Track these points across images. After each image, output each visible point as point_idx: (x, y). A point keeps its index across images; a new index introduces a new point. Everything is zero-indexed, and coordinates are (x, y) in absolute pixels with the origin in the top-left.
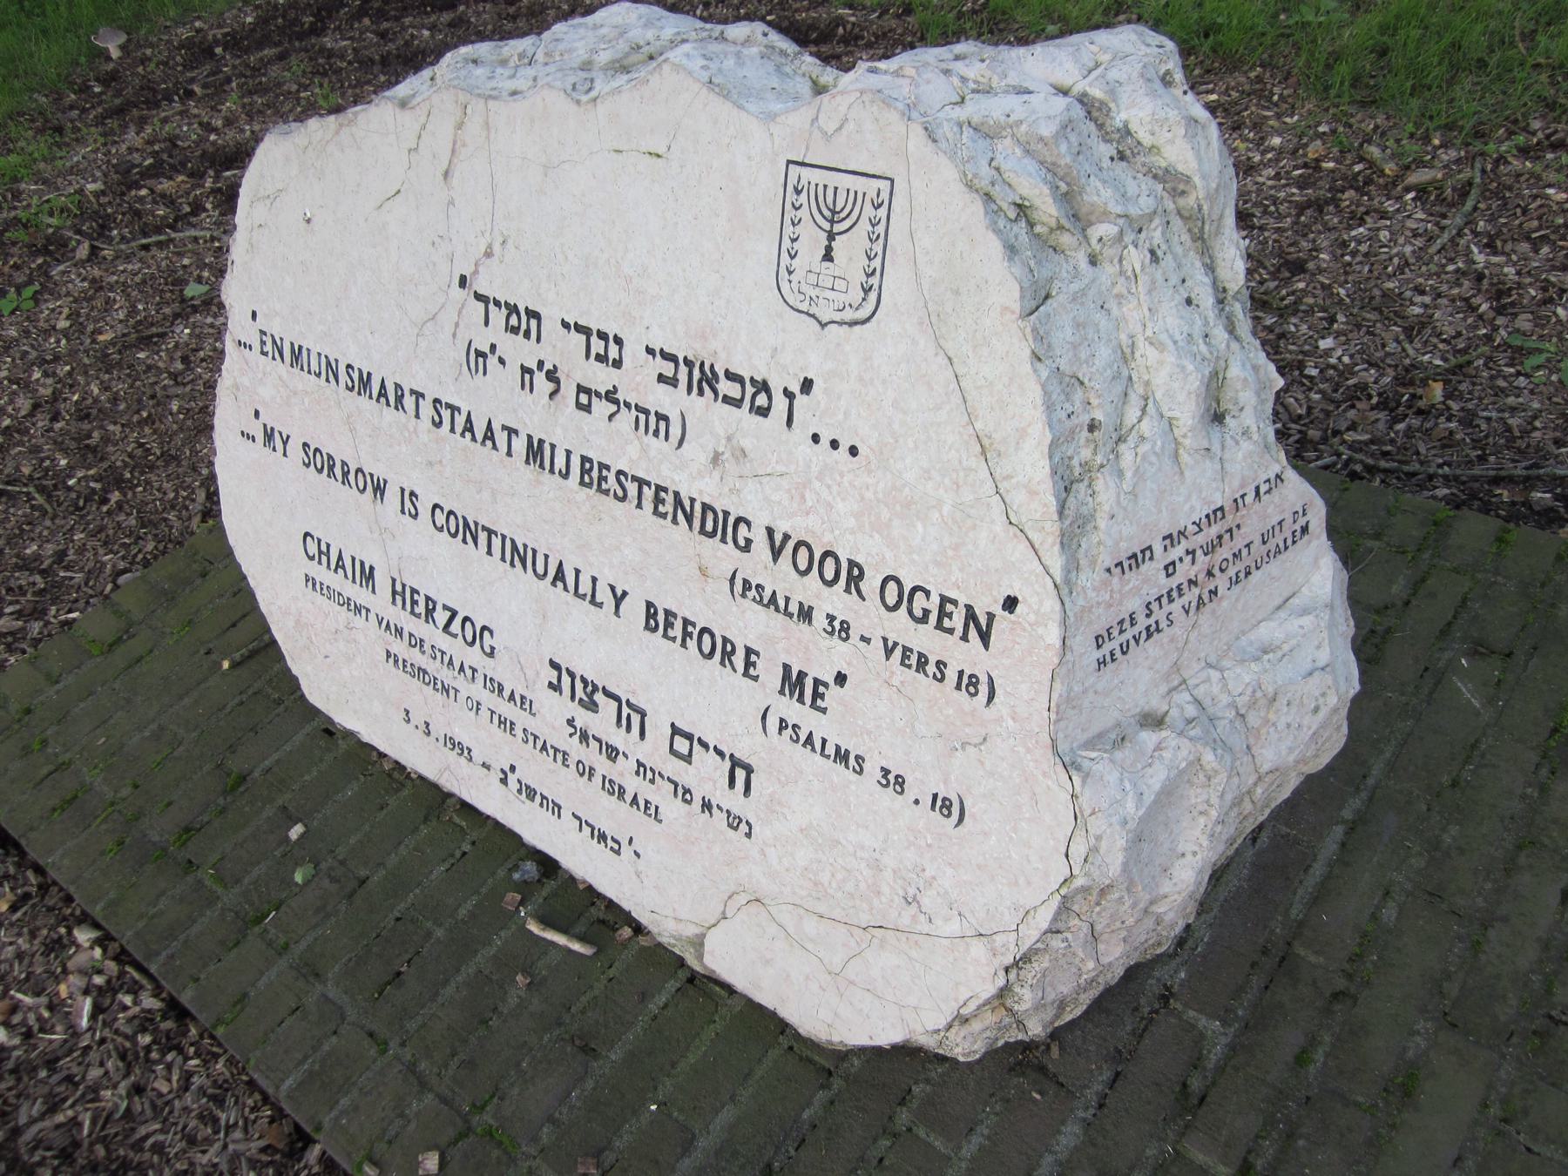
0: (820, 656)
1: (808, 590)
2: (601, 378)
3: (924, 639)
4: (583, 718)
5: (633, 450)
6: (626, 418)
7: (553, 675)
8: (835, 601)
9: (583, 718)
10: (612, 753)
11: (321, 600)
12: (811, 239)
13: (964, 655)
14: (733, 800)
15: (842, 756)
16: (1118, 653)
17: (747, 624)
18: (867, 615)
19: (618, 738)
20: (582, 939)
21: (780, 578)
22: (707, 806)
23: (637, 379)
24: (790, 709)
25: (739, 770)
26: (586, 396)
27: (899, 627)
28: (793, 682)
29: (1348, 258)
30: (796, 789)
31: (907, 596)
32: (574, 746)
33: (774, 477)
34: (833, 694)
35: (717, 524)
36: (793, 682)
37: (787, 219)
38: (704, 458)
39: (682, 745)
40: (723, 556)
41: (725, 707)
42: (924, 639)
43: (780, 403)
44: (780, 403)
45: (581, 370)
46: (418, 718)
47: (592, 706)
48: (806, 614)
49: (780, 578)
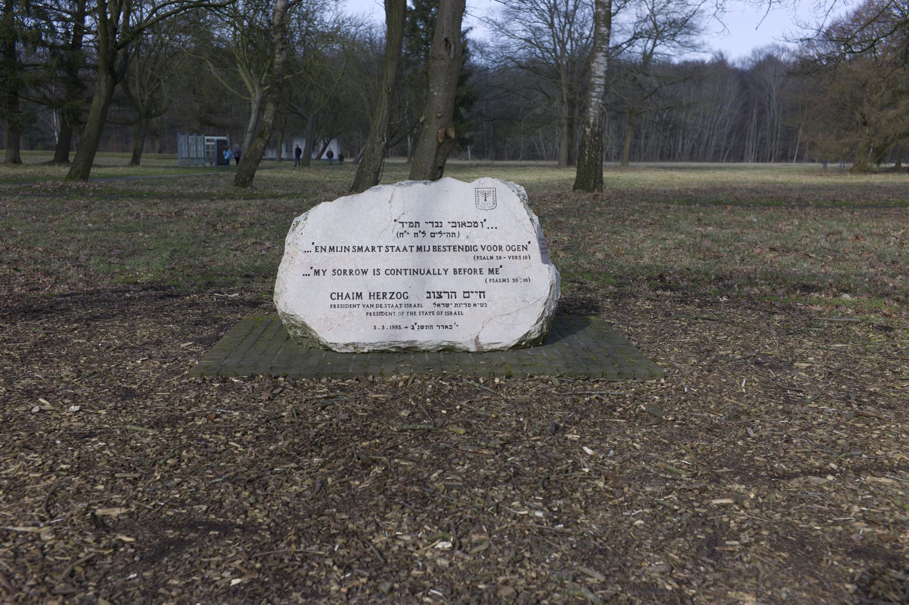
0: (495, 264)
1: (492, 253)
2: (437, 230)
3: (516, 253)
4: (438, 301)
5: (447, 241)
6: (444, 236)
7: (428, 295)
8: (498, 253)
9: (438, 301)
10: (447, 305)
11: (339, 310)
12: (482, 199)
13: (523, 253)
14: (482, 301)
15: (504, 280)
16: (388, 296)
17: (478, 264)
18: (504, 253)
19: (449, 301)
20: (890, 162)
21: (486, 253)
22: (475, 305)
23: (447, 228)
24: (492, 276)
25: (482, 293)
26: (433, 235)
27: (511, 253)
28: (491, 271)
29: (263, 252)
30: (495, 291)
31: (511, 248)
32: (437, 309)
33: (477, 237)
34: (500, 270)
35: (468, 249)
36: (491, 271)
37: (477, 196)
38: (464, 238)
39: (466, 295)
40: (471, 254)
41: (476, 282)
42: (516, 253)
43: (480, 224)
44: (480, 224)
45: (430, 229)
46: (379, 326)
47: (441, 297)
48: (492, 258)
49: (486, 253)
